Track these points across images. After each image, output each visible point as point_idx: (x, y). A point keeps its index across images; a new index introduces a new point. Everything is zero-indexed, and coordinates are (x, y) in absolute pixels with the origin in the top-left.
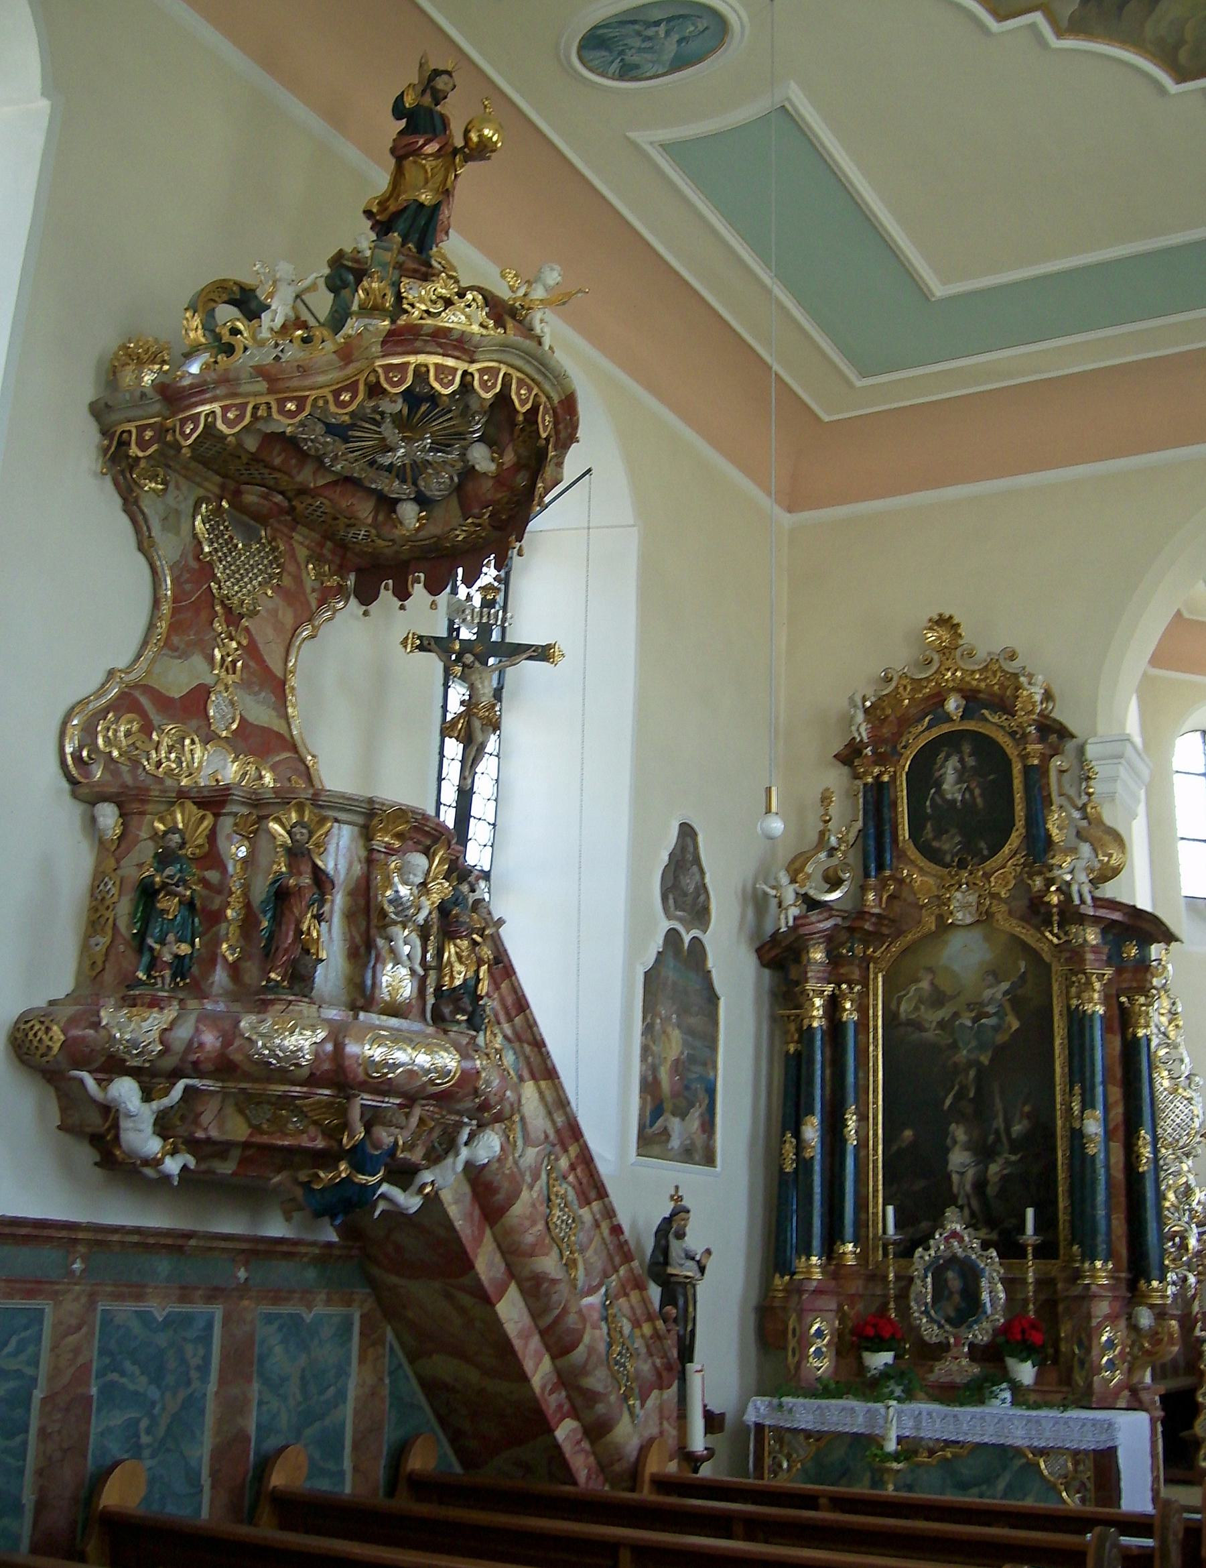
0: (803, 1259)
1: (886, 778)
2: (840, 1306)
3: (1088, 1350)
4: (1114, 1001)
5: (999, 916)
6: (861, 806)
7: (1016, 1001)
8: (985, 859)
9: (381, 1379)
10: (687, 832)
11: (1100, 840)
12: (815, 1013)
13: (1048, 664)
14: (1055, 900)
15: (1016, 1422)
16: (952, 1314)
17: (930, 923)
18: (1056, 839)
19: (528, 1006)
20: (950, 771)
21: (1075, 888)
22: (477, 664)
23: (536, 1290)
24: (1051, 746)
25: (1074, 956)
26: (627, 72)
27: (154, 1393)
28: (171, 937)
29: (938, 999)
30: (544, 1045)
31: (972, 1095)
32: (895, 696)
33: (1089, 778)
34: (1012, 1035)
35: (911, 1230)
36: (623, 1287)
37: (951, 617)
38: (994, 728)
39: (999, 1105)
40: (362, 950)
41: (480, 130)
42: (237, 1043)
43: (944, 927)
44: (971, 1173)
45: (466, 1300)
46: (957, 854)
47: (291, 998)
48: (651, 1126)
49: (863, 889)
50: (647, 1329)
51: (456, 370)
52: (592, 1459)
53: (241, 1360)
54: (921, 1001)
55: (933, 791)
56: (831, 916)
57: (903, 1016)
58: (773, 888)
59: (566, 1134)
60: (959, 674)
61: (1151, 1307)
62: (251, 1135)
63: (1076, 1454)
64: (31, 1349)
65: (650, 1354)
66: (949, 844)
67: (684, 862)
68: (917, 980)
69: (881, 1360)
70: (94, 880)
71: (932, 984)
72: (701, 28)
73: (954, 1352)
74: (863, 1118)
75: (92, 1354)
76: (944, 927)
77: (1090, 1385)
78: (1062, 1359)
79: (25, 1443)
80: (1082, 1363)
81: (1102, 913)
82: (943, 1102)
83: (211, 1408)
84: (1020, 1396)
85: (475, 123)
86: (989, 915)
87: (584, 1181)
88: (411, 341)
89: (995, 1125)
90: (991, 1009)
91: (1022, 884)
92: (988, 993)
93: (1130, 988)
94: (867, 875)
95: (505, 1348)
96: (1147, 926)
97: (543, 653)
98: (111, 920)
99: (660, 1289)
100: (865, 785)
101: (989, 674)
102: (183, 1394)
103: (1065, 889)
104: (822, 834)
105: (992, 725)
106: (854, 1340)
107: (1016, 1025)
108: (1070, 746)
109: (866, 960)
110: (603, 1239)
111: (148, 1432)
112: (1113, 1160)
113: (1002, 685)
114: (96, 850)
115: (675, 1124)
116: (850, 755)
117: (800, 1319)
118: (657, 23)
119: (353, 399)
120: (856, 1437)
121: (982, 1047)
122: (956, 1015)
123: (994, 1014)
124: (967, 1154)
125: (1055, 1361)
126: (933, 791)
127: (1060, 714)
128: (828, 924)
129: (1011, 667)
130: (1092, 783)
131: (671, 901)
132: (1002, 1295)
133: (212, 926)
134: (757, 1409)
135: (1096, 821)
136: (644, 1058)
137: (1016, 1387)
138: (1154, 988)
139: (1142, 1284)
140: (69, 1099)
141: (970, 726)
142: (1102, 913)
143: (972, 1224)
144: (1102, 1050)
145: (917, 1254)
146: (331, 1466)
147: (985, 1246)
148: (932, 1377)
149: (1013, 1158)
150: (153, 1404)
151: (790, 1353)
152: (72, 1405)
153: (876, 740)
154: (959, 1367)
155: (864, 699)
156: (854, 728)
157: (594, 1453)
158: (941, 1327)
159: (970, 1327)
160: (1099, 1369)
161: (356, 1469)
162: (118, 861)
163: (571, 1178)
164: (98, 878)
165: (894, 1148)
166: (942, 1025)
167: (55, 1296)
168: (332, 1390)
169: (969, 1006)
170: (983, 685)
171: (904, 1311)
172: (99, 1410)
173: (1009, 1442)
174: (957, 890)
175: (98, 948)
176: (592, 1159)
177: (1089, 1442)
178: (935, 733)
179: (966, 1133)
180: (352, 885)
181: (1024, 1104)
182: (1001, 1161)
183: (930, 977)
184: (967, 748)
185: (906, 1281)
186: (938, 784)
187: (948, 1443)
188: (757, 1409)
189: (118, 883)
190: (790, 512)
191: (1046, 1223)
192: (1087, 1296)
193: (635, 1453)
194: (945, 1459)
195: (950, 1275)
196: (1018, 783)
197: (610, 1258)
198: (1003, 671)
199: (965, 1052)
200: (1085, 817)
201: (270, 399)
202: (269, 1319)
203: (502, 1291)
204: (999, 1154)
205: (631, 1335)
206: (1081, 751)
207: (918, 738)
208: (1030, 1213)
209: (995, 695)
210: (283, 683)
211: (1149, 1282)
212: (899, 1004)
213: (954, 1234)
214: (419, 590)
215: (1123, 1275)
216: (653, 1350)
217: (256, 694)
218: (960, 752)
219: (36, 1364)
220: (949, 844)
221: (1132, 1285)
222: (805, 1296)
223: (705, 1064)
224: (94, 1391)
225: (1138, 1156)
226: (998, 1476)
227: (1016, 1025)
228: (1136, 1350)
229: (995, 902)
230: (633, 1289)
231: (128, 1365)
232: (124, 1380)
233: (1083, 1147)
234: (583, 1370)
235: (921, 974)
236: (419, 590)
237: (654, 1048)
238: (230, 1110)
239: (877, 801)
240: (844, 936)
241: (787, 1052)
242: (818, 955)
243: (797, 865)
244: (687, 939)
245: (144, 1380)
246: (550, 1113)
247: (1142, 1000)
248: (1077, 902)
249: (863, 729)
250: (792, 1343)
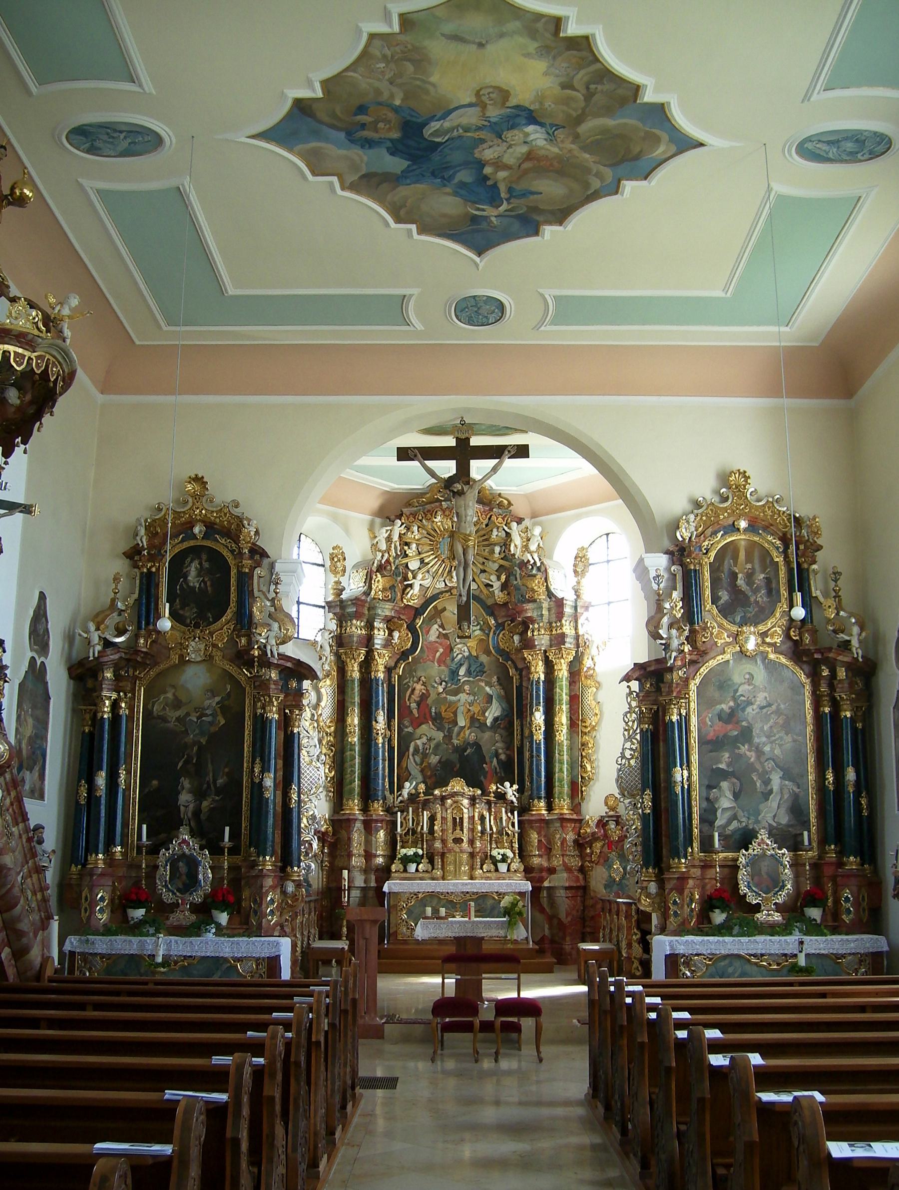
0: (94, 855)
1: (154, 570)
3: (261, 904)
6: (138, 585)
7: (224, 708)
8: (210, 624)
10: (42, 597)
11: (283, 620)
12: (106, 709)
13: (259, 514)
14: (256, 653)
16: (181, 886)
17: (175, 659)
20: (193, 569)
21: (269, 648)
24: (255, 561)
25: (262, 685)
26: (92, 150)
29: (177, 704)
32: (164, 520)
34: (220, 728)
36: (29, 872)
38: (222, 546)
41: (22, 190)
43: (183, 662)
44: (191, 806)
46: (194, 619)
49: (137, 636)
56: (119, 652)
57: (155, 714)
58: (86, 633)
59: (10, 785)
60: (203, 512)
61: (293, 881)
63: (257, 960)
65: (39, 910)
66: (189, 613)
67: (40, 615)
68: (165, 692)
69: (139, 913)
71: (174, 694)
72: (146, 140)
73: (181, 908)
74: (129, 772)
76: (183, 662)
78: (242, 911)
80: (256, 912)
84: (220, 931)
86: (211, 657)
90: (208, 712)
91: (232, 642)
92: (207, 702)
96: (303, 671)
100: (142, 573)
101: (223, 514)
103: (263, 648)
104: (113, 601)
105: (222, 545)
106: (121, 905)
107: (223, 722)
108: (266, 562)
109: (136, 678)
113: (229, 522)
115: (27, 775)
116: (133, 554)
117: (91, 890)
118: (121, 132)
121: (202, 733)
122: (188, 714)
125: (239, 912)
128: (116, 657)
129: (236, 512)
130: (279, 586)
132: (210, 876)
135: (278, 609)
137: (218, 926)
143: (193, 834)
145: (161, 853)
147: (202, 848)
148: (168, 923)
149: (217, 798)
151: (83, 911)
153: (151, 546)
155: (146, 521)
156: (138, 538)
158: (174, 893)
159: (191, 894)
163: (11, 810)
166: (178, 719)
169: (196, 709)
170: (218, 520)
173: (221, 955)
177: (266, 953)
178: (186, 545)
181: (225, 767)
183: (173, 690)
184: (204, 557)
186: (185, 576)
188: (72, 943)
191: (234, 836)
192: (261, 875)
194: (184, 967)
196: (233, 581)
198: (230, 513)
200: (273, 605)
206: (272, 566)
208: (227, 829)
209: (228, 527)
211: (292, 868)
212: (153, 706)
213: (184, 841)
215: (279, 864)
218: (200, 558)
220: (189, 613)
221: (283, 869)
225: (290, 799)
234: (19, 919)
239: (148, 583)
240: (123, 663)
241: (84, 731)
242: (109, 675)
243: (99, 619)
247: (297, 712)
248: (269, 655)
249: (144, 540)
250: (85, 905)
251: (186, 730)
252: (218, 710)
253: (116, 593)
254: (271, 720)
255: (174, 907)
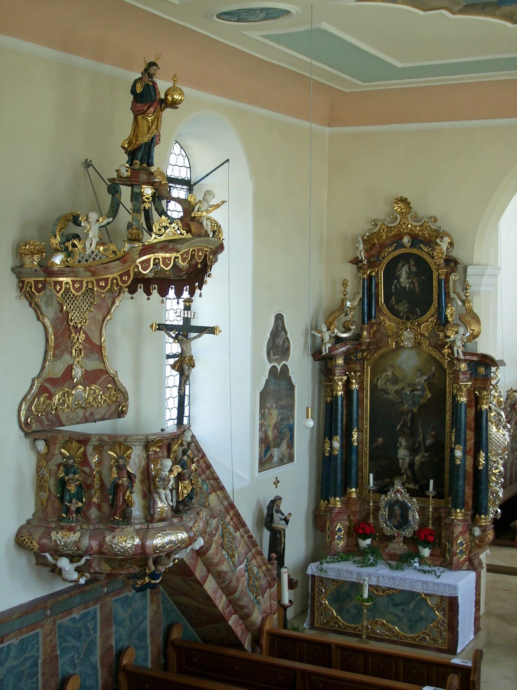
2: (349, 517)
3: (452, 546)
4: (473, 394)
5: (423, 345)
7: (430, 384)
9: (159, 606)
10: (279, 318)
15: (418, 583)
16: (396, 524)
18: (450, 320)
19: (211, 466)
20: (404, 272)
22: (184, 339)
23: (219, 577)
24: (451, 267)
27: (79, 644)
28: (74, 501)
29: (395, 380)
30: (219, 479)
31: (409, 425)
33: (467, 289)
35: (381, 482)
36: (254, 556)
37: (406, 199)
38: (425, 254)
39: (421, 430)
40: (148, 494)
42: (105, 546)
43: (399, 347)
44: (407, 459)
45: (193, 584)
46: (406, 313)
47: (124, 527)
48: (264, 457)
50: (264, 568)
51: (171, 258)
52: (243, 626)
53: (108, 620)
54: (387, 380)
55: (395, 281)
57: (379, 387)
60: (409, 226)
62: (111, 571)
64: (36, 646)
65: (265, 576)
69: (366, 543)
70: (37, 468)
71: (393, 373)
75: (57, 641)
76: (399, 347)
77: (452, 560)
79: (38, 678)
81: (468, 357)
82: (396, 428)
83: (99, 642)
85: (171, 92)
87: (237, 522)
88: (151, 250)
89: (419, 439)
90: (419, 387)
92: (417, 380)
93: (480, 388)
94: (363, 323)
95: (208, 598)
96: (488, 362)
97: (212, 330)
98: (47, 488)
99: (269, 532)
102: (88, 640)
105: (423, 252)
107: (429, 395)
109: (363, 359)
110: (245, 541)
111: (78, 658)
112: (467, 463)
113: (429, 234)
114: (36, 455)
117: (331, 524)
119: (129, 278)
120: (353, 583)
121: (414, 404)
122: (403, 389)
123: (421, 390)
124: (406, 451)
126: (395, 281)
127: (455, 253)
131: (272, 353)
132: (418, 517)
133: (89, 490)
134: (312, 569)
136: (260, 429)
138: (492, 385)
139: (477, 516)
140: (41, 562)
141: (414, 251)
142: (468, 357)
144: (467, 416)
146: (143, 644)
149: (426, 454)
150: (78, 648)
151: (327, 529)
152: (52, 660)
154: (398, 547)
157: (244, 624)
158: (391, 529)
159: (403, 530)
160: (456, 554)
161: (152, 643)
162: (47, 463)
163: (231, 523)
164: (39, 468)
165: (374, 446)
166: (396, 392)
167: (42, 627)
168: (141, 617)
169: (409, 385)
170: (421, 233)
171: (376, 518)
172: (60, 657)
174: (405, 331)
175: (43, 497)
176: (240, 515)
178: (397, 253)
179: (406, 441)
180: (142, 469)
181: (432, 431)
182: (421, 455)
183: (392, 370)
185: (377, 509)
186: (398, 278)
187: (390, 589)
188: (312, 569)
189: (48, 472)
190: (329, 126)
193: (260, 623)
195: (396, 507)
197: (248, 547)
198: (430, 227)
199: (406, 406)
201: (92, 279)
202: (116, 601)
203: (205, 579)
204: (420, 452)
205: (258, 572)
207: (390, 254)
208: (431, 482)
209: (426, 238)
210: (101, 347)
211: (480, 515)
212: (377, 381)
213: (398, 491)
214: (155, 293)
216: (266, 574)
217: (89, 358)
218: (409, 263)
219: (38, 651)
220: (403, 307)
221: (473, 517)
222: (333, 515)
223: (288, 418)
224: (58, 652)
226: (410, 602)
227: (429, 395)
228: (473, 544)
229: (422, 338)
230: (258, 555)
231: (69, 638)
232: (68, 644)
233: (454, 461)
234: (239, 599)
235: (388, 368)
236: (155, 293)
237: (265, 423)
238: (103, 562)
241: (327, 401)
242: (340, 361)
243: (330, 320)
244: (279, 368)
245: (75, 641)
246: (222, 502)
247: (485, 393)
250: (328, 533)
251: (402, 401)
252: (426, 387)
253: (345, 295)
254: (461, 404)
255: (391, 538)
